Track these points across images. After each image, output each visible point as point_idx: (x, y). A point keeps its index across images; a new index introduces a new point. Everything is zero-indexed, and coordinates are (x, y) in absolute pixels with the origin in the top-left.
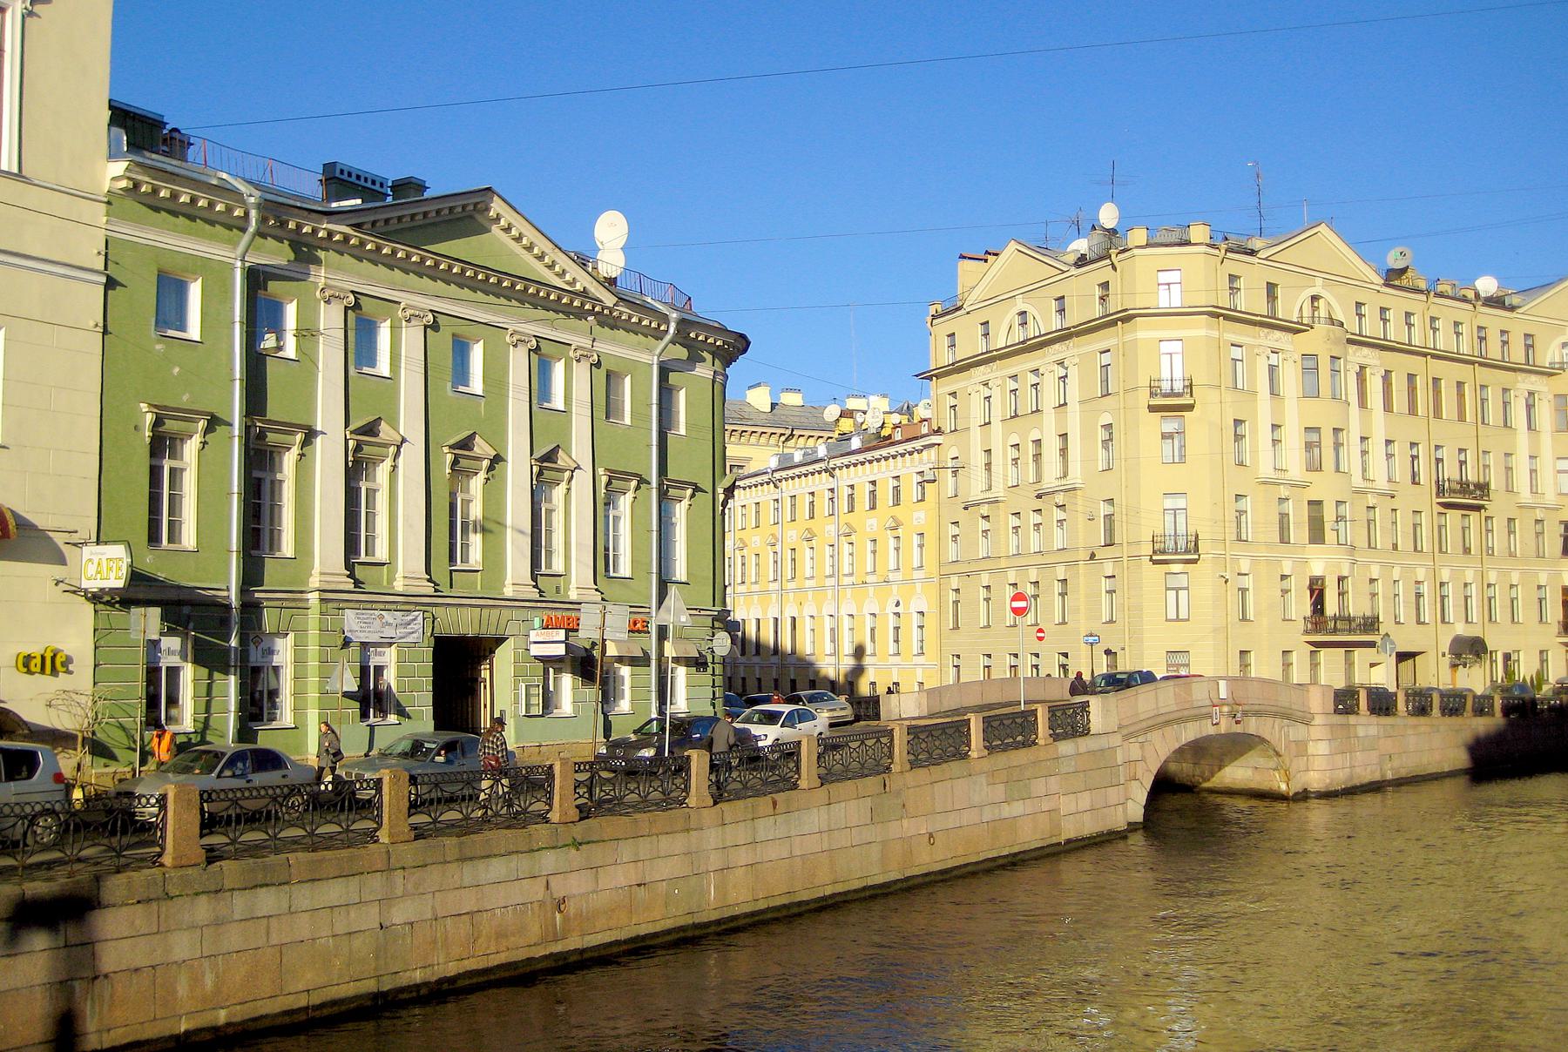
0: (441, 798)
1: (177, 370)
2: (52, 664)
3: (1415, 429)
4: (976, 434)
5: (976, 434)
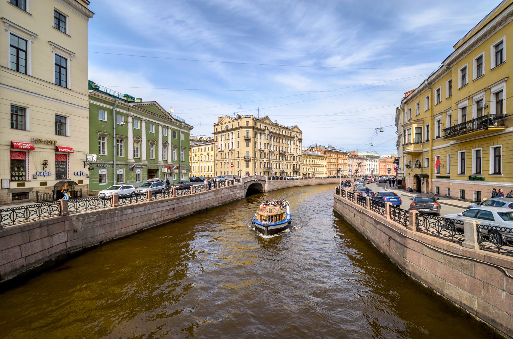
1: (103, 126)
4: (220, 141)
5: (220, 141)
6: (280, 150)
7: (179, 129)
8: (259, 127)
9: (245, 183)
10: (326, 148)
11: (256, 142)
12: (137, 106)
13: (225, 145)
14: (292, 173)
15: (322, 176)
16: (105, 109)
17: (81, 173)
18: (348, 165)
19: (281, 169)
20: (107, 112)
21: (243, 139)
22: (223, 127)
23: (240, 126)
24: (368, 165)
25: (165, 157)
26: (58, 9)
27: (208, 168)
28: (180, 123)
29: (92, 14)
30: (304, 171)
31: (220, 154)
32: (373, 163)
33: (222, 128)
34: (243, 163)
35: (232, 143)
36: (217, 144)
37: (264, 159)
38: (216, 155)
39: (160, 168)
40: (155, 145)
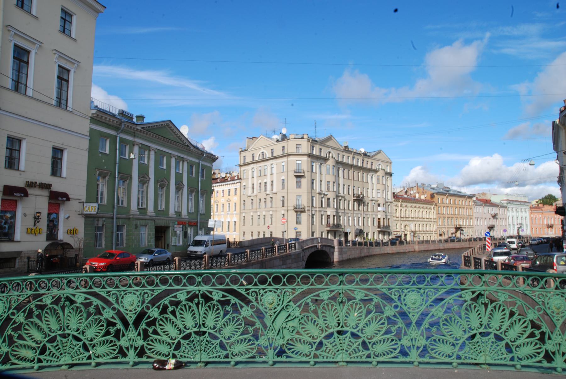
0: (366, 242)
1: (104, 161)
2: (551, 226)
3: (350, 183)
6: (355, 193)
7: (197, 161)
8: (318, 154)
9: (302, 250)
10: (433, 189)
11: (313, 180)
12: (146, 129)
13: (259, 185)
14: (376, 234)
15: (429, 239)
16: (108, 136)
17: (75, 230)
18: (474, 218)
19: (357, 227)
20: (109, 140)
21: (292, 174)
22: (255, 155)
23: (286, 152)
24: (511, 218)
25: (142, 203)
26: (66, 7)
27: (229, 225)
28: (201, 154)
29: (104, 8)
30: (398, 230)
31: (251, 201)
32: (520, 215)
33: (253, 157)
34: (292, 216)
35: (272, 181)
36: (244, 184)
37: (328, 209)
38: (242, 202)
39: (171, 225)
40: (165, 188)
